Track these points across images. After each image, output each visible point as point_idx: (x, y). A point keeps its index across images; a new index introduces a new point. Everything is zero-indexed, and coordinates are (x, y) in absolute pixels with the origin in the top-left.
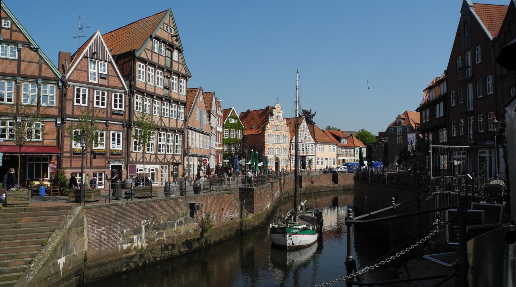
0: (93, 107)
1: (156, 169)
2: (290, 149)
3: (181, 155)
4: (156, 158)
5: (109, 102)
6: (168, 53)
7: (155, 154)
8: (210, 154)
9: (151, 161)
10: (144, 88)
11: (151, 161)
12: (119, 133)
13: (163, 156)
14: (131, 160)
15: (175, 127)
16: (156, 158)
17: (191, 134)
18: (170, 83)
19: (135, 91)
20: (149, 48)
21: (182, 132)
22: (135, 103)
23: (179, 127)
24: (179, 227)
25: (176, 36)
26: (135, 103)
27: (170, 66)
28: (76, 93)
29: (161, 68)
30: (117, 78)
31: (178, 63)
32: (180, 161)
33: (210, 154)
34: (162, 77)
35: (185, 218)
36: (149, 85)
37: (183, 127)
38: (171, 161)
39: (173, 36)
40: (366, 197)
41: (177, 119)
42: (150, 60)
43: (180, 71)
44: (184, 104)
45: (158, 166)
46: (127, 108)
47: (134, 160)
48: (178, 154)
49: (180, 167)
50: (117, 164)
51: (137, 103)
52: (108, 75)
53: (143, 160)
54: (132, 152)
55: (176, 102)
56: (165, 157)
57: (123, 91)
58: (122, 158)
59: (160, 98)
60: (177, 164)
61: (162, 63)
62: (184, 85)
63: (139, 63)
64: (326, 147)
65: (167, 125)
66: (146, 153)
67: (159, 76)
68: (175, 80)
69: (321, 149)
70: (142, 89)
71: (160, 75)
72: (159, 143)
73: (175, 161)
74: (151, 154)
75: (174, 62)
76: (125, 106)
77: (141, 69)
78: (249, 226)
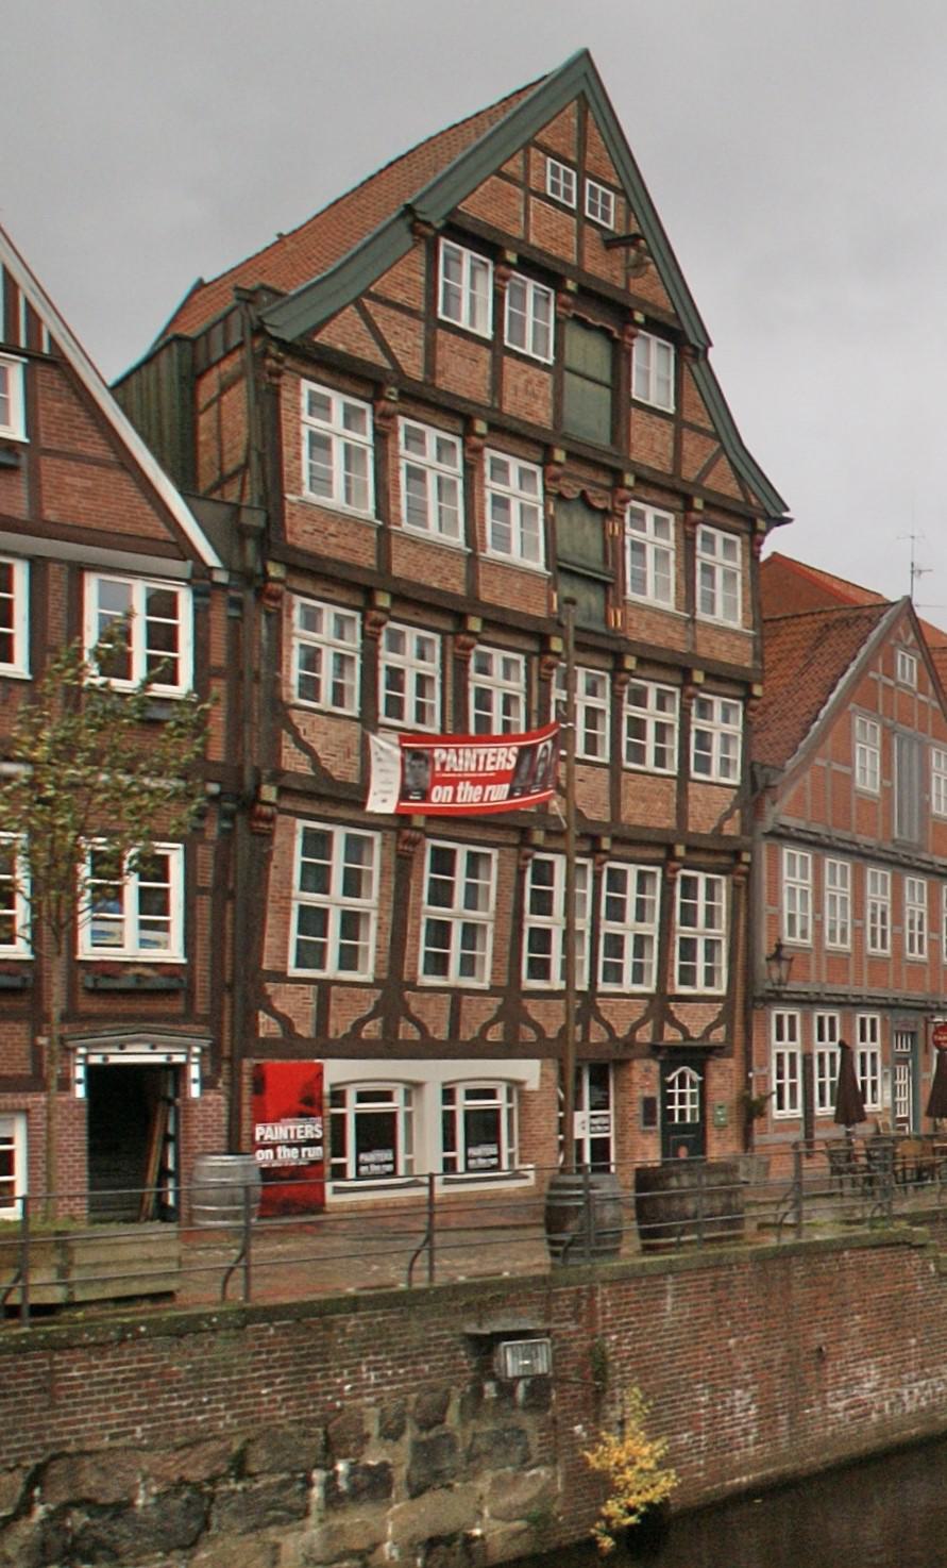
1: (515, 1086)
3: (728, 1000)
6: (589, 352)
7: (493, 991)
9: (467, 1034)
14: (267, 1026)
15: (670, 823)
17: (793, 871)
19: (275, 571)
21: (730, 857)
22: (296, 657)
24: (356, 1520)
26: (296, 657)
27: (602, 438)
28: (383, 691)
32: (718, 1036)
35: (418, 1446)
37: (732, 828)
38: (645, 1036)
39: (611, 242)
43: (690, 473)
44: (726, 678)
45: (529, 1071)
46: (218, 688)
48: (700, 988)
49: (724, 1079)
50: (139, 1055)
51: (311, 659)
54: (280, 976)
55: (678, 668)
57: (183, 568)
58: (188, 1016)
60: (698, 1055)
63: (307, 386)
66: (412, 985)
70: (453, 596)
72: (608, 927)
73: (671, 1035)
75: (636, 415)
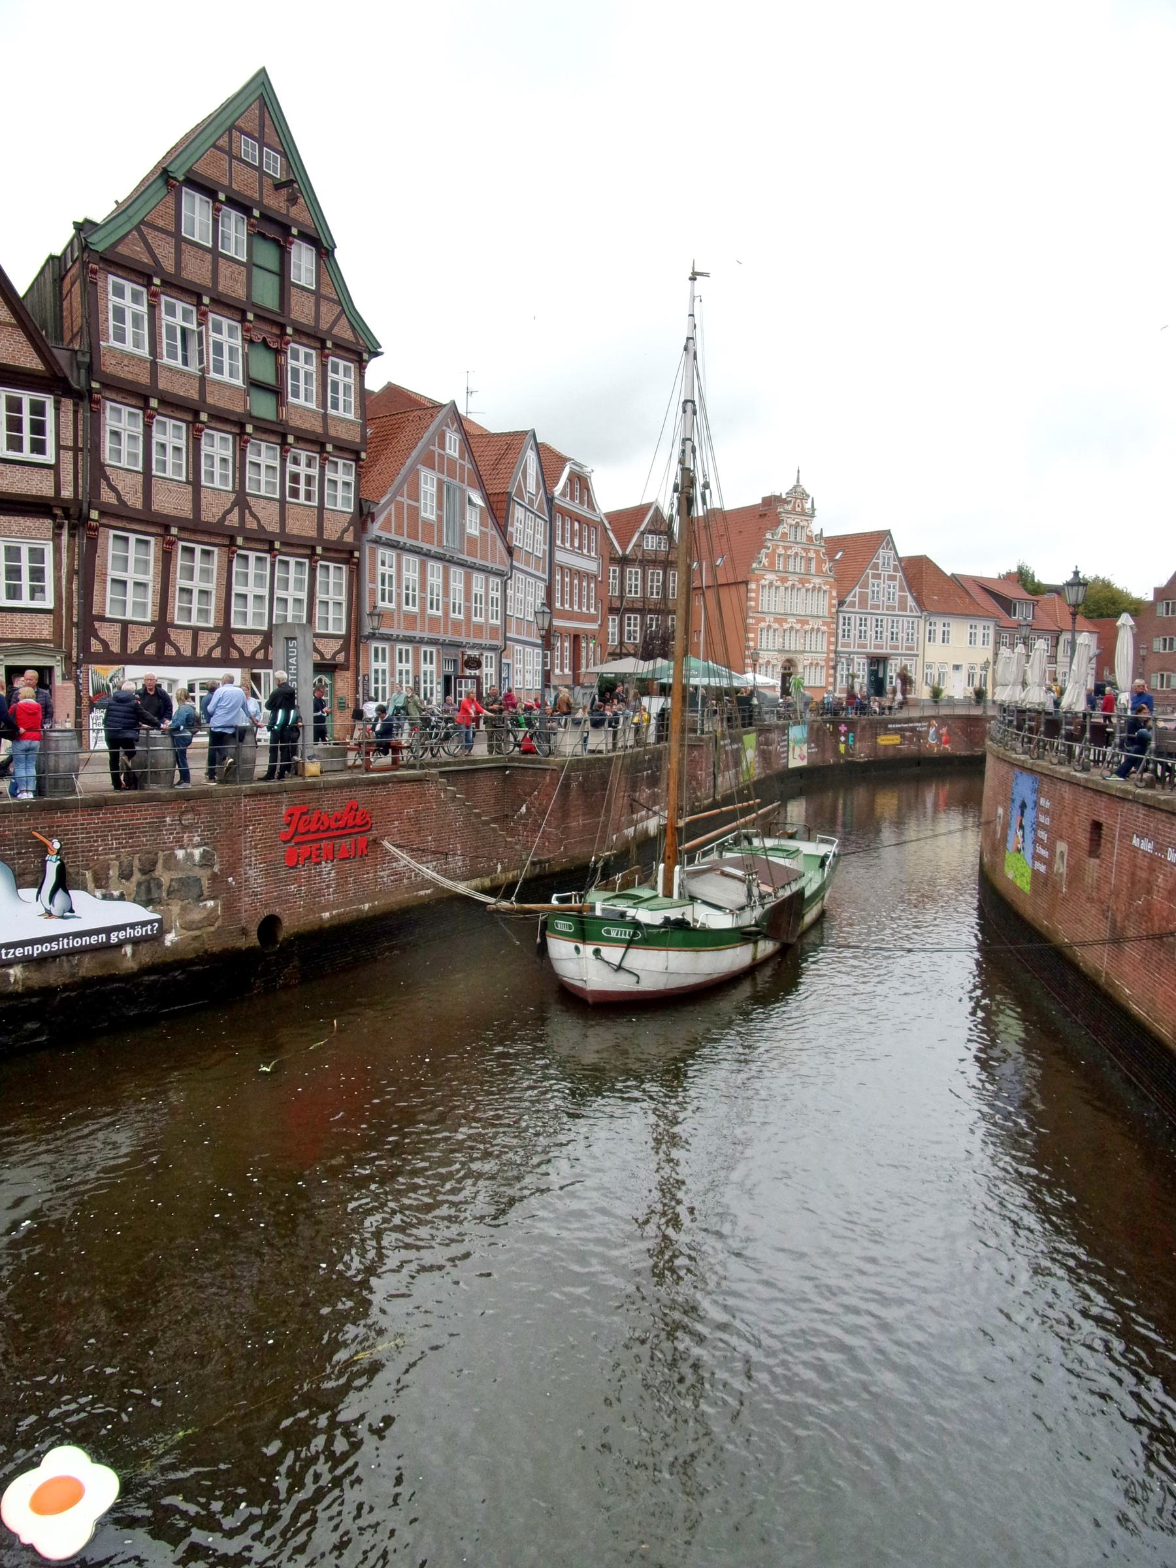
6: (267, 255)
8: (506, 639)
9: (202, 653)
11: (202, 653)
18: (280, 371)
20: (161, 223)
21: (347, 555)
25: (289, 183)
29: (236, 310)
32: (341, 658)
33: (506, 639)
34: (238, 342)
36: (334, 418)
41: (282, 502)
53: (160, 649)
55: (317, 442)
59: (238, 425)
61: (233, 286)
62: (351, 381)
63: (111, 279)
64: (959, 630)
65: (273, 527)
67: (224, 338)
68: (302, 362)
69: (939, 636)
71: (227, 335)
74: (196, 631)
75: (293, 291)
76: (59, 447)
77: (127, 302)
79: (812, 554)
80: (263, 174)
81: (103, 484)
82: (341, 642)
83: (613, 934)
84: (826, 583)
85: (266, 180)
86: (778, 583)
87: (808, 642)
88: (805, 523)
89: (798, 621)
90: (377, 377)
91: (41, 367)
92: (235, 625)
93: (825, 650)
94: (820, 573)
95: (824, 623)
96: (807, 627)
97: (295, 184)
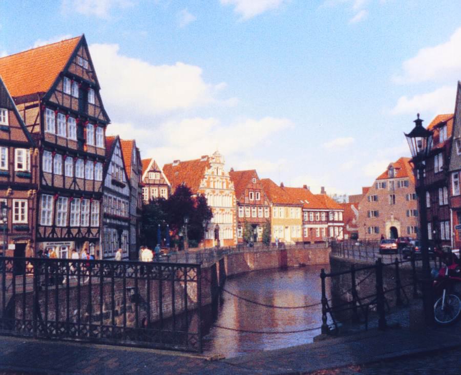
0: (14, 172)
2: (263, 223)
4: (69, 232)
5: (11, 159)
7: (67, 227)
10: (95, 153)
12: (23, 201)
13: (76, 230)
15: (92, 190)
16: (69, 232)
23: (96, 190)
30: (21, 131)
31: (95, 106)
37: (101, 191)
40: (159, 225)
42: (61, 104)
43: (96, 116)
47: (42, 236)
52: (10, 127)
53: (53, 236)
56: (79, 231)
65: (82, 189)
73: (91, 236)
78: (234, 345)
79: (224, 180)
80: (83, 68)
81: (43, 178)
82: (98, 229)
83: (176, 348)
84: (231, 193)
85: (84, 70)
86: (212, 193)
87: (224, 219)
88: (221, 167)
89: (220, 210)
90: (111, 131)
91: (27, 141)
92: (71, 225)
93: (232, 222)
94: (228, 188)
95: (231, 210)
96: (224, 212)
97: (92, 71)
